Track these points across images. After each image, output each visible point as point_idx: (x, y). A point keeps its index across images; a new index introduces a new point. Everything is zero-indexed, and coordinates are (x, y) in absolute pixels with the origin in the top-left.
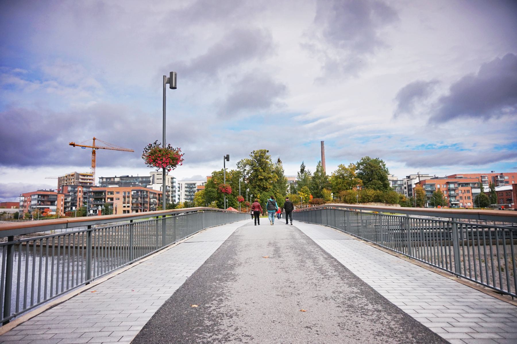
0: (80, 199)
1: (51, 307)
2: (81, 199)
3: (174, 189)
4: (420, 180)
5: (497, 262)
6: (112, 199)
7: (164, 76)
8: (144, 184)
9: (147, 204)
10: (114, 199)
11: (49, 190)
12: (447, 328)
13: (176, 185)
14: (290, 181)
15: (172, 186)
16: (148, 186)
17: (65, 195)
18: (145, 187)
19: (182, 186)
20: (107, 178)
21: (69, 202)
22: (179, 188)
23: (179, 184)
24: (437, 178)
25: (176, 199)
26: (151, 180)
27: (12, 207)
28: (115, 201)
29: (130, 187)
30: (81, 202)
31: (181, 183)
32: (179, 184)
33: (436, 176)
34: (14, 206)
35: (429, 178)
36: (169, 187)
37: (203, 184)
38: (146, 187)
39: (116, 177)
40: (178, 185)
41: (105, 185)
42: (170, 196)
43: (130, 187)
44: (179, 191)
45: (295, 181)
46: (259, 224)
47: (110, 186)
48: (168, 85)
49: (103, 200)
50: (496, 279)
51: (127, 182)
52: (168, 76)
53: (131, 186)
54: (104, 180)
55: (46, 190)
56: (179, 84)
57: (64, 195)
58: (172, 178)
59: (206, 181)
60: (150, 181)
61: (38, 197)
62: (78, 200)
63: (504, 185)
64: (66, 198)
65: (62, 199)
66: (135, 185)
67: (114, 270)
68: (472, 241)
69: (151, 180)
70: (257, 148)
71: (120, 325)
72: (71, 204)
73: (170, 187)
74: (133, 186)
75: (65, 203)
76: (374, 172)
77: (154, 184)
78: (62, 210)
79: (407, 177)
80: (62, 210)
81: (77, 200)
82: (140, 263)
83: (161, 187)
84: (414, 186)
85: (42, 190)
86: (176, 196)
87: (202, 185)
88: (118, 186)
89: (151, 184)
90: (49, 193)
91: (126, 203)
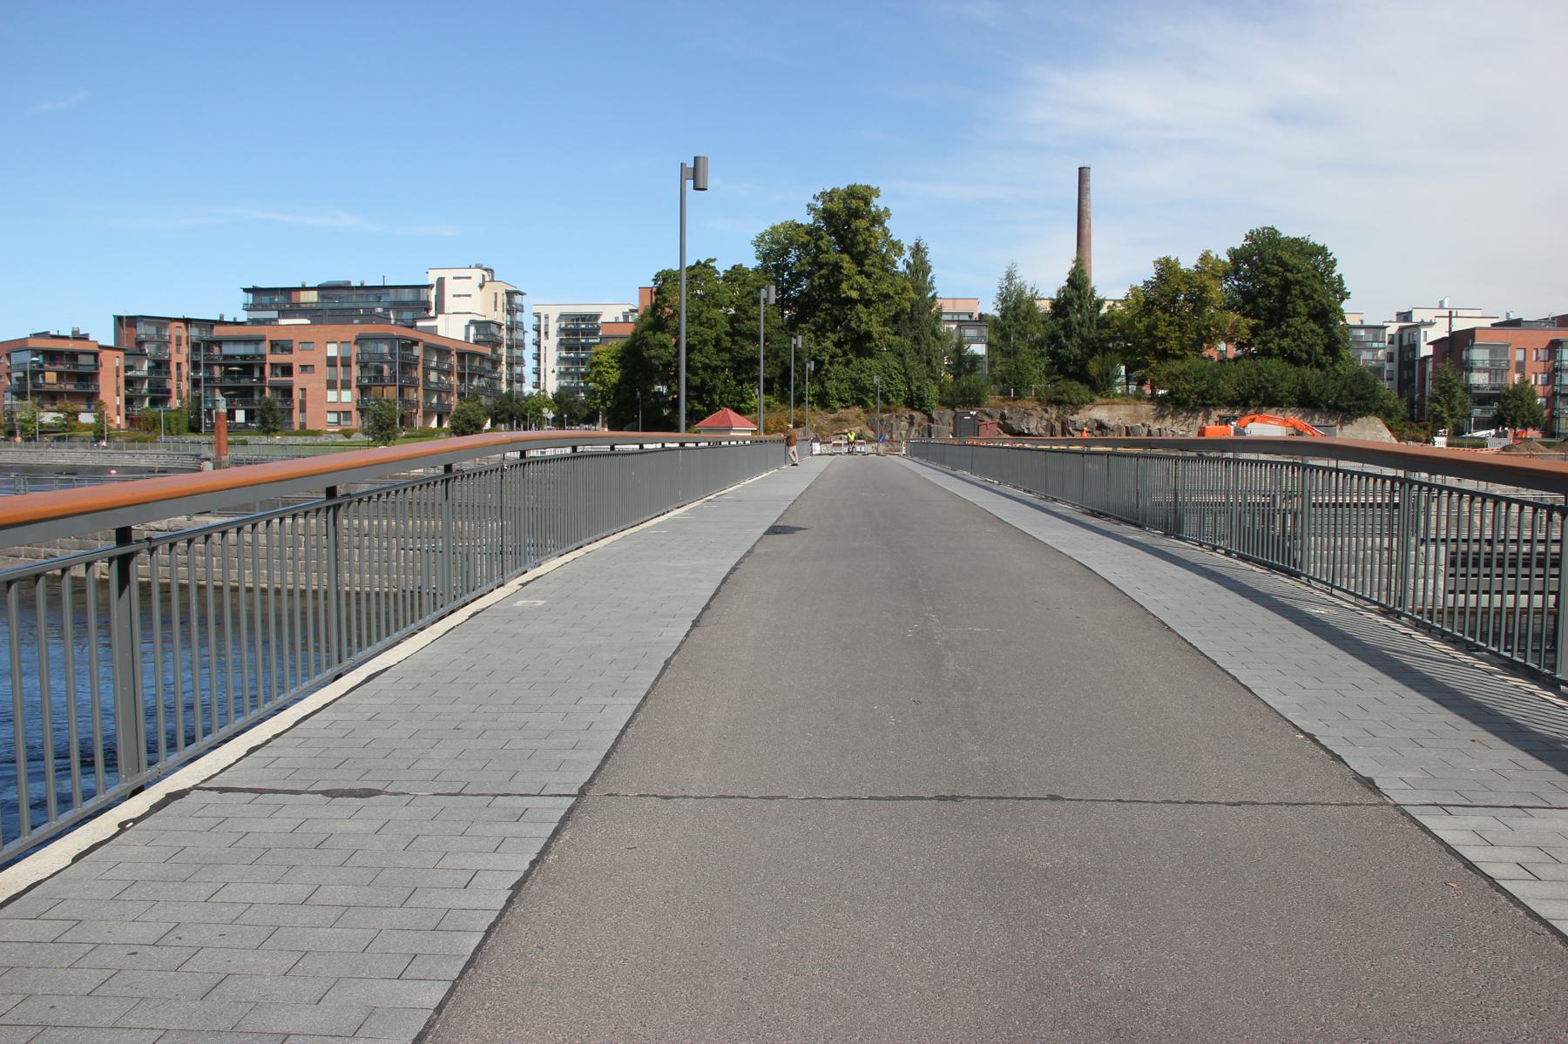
0: (179, 365)
1: (370, 678)
2: (186, 369)
3: (517, 335)
4: (1453, 330)
6: (287, 370)
7: (682, 164)
8: (407, 315)
9: (416, 388)
10: (296, 369)
11: (69, 334)
12: (1529, 878)
13: (527, 320)
14: (959, 314)
15: (512, 322)
16: (419, 324)
17: (125, 354)
18: (411, 327)
19: (546, 326)
21: (142, 379)
22: (538, 329)
23: (538, 316)
24: (1517, 323)
25: (525, 374)
26: (433, 300)
30: (184, 378)
31: (543, 311)
32: (538, 316)
33: (1512, 317)
35: (1487, 323)
36: (499, 326)
37: (626, 316)
38: (412, 326)
39: (304, 289)
42: (504, 362)
43: (352, 323)
45: (976, 316)
48: (690, 183)
49: (257, 374)
51: (346, 305)
52: (691, 165)
53: (356, 321)
55: (61, 334)
56: (713, 180)
57: (121, 354)
58: (510, 295)
59: (636, 305)
60: (428, 302)
62: (173, 369)
64: (131, 363)
65: (118, 368)
66: (369, 317)
68: (1546, 558)
69: (433, 300)
71: (58, 940)
72: (150, 385)
73: (504, 327)
74: (361, 323)
75: (129, 382)
76: (1296, 291)
77: (443, 312)
78: (118, 407)
79: (1399, 314)
80: (118, 407)
81: (168, 372)
82: (523, 585)
84: (1426, 350)
85: (45, 335)
86: (526, 363)
87: (621, 320)
88: (308, 322)
89: (432, 313)
90: (71, 346)
91: (339, 385)
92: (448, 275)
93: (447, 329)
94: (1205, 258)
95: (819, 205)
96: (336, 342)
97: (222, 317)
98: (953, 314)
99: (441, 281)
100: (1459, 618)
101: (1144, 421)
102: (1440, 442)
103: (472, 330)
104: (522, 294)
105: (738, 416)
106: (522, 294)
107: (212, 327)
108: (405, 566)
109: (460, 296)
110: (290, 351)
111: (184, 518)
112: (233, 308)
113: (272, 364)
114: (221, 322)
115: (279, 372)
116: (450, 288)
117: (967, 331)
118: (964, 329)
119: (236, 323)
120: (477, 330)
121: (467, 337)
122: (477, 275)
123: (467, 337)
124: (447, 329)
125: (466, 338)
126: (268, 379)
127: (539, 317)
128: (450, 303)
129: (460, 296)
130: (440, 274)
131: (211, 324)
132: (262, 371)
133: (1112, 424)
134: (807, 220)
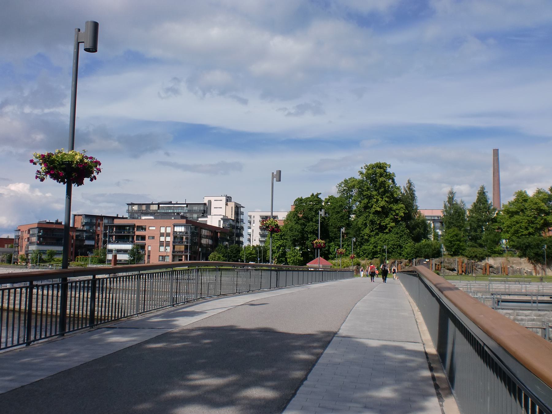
5: (120, 301)
10: (147, 238)
14: (434, 216)
20: (140, 205)
27: (6, 245)
28: (147, 241)
29: (171, 219)
32: (250, 217)
34: (8, 244)
40: (249, 219)
41: (136, 215)
43: (171, 219)
44: (250, 228)
46: (374, 282)
47: (143, 218)
50: (7, 301)
54: (135, 208)
61: (39, 232)
63: (122, 243)
67: (106, 322)
70: (64, 185)
78: (72, 252)
83: (220, 221)
88: (153, 218)
92: (212, 199)
93: (211, 222)
94: (539, 192)
95: (364, 171)
96: (164, 227)
97: (8, 237)
98: (431, 216)
99: (210, 202)
100: (176, 261)
101: (511, 265)
102: (107, 239)
103: (222, 222)
104: (243, 207)
105: (326, 261)
106: (243, 207)
107: (113, 220)
108: (155, 306)
109: (217, 208)
110: (145, 229)
111: (96, 299)
112: (123, 212)
113: (137, 236)
114: (117, 218)
115: (140, 239)
116: (214, 204)
117: (436, 224)
118: (435, 223)
119: (123, 218)
120: (224, 222)
121: (220, 225)
122: (224, 199)
123: (220, 225)
124: (211, 222)
125: (219, 225)
126: (136, 241)
127: (251, 217)
128: (213, 211)
129: (217, 208)
130: (210, 198)
131: (113, 218)
132: (133, 238)
133: (495, 266)
134: (359, 177)
